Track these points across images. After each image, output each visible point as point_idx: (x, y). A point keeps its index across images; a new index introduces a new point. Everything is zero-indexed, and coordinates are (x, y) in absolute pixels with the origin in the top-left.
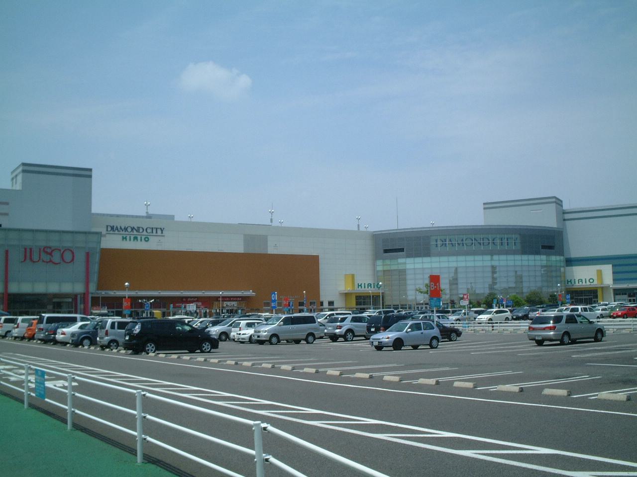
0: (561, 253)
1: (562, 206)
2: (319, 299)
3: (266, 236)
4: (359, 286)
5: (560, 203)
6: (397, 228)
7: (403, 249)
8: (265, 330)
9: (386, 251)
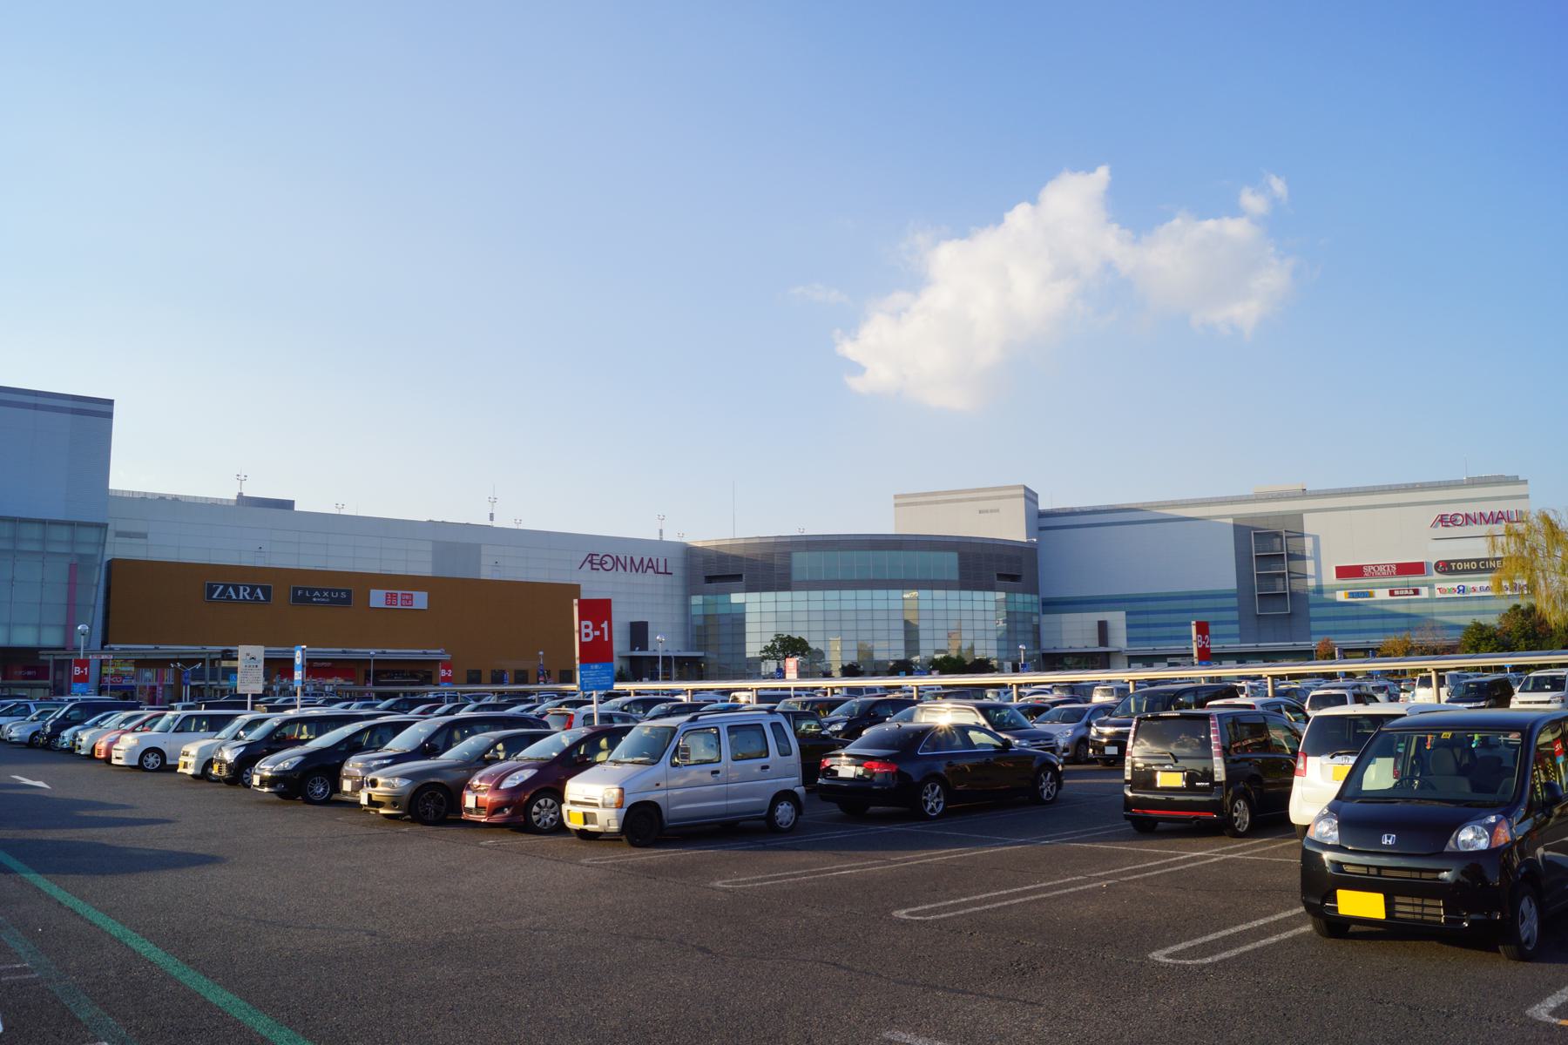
0: (1033, 589)
1: (1036, 503)
3: (478, 546)
5: (1034, 498)
7: (741, 576)
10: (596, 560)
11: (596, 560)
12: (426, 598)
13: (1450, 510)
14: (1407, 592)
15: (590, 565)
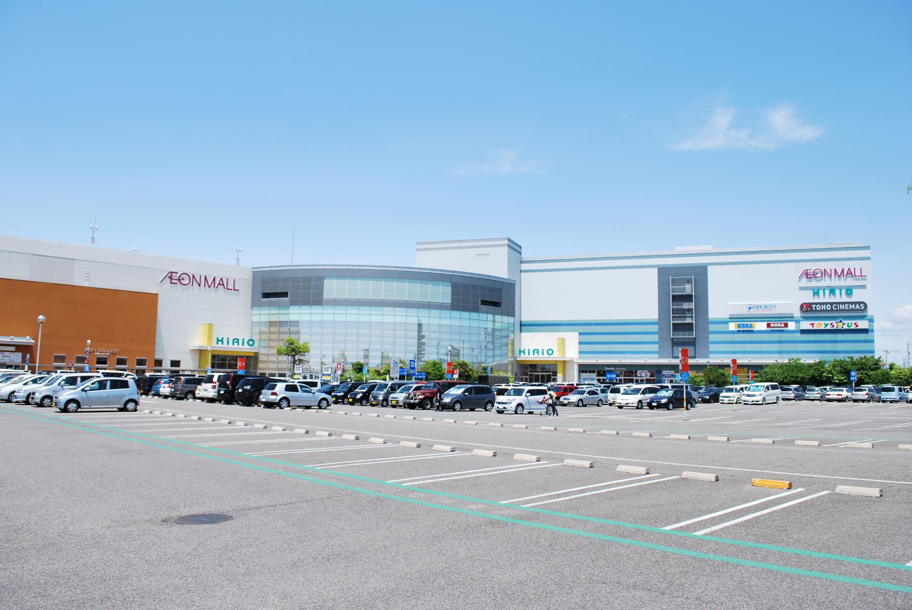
0: (511, 313)
1: (520, 253)
2: (154, 356)
4: (218, 340)
5: (518, 249)
7: (287, 293)
8: (41, 390)
9: (266, 295)
10: (176, 276)
11: (176, 276)
12: (324, 296)
13: (812, 267)
14: (779, 325)
15: (169, 280)
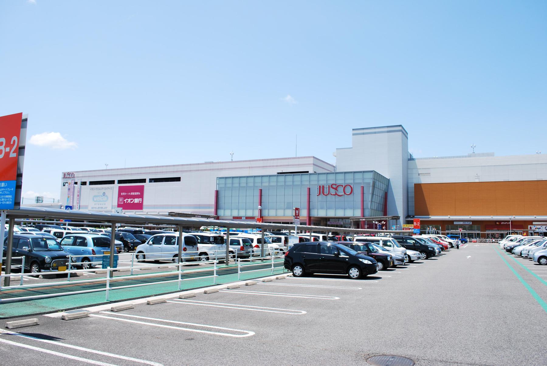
6: (295, 157)
